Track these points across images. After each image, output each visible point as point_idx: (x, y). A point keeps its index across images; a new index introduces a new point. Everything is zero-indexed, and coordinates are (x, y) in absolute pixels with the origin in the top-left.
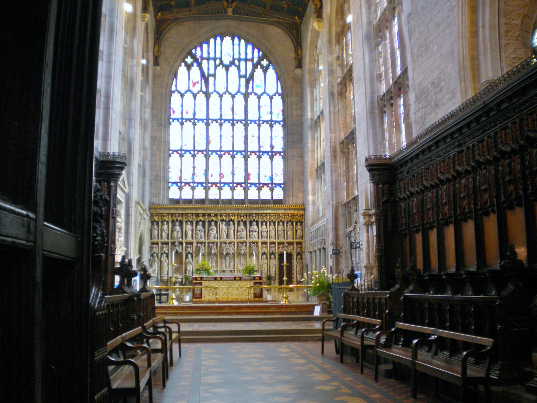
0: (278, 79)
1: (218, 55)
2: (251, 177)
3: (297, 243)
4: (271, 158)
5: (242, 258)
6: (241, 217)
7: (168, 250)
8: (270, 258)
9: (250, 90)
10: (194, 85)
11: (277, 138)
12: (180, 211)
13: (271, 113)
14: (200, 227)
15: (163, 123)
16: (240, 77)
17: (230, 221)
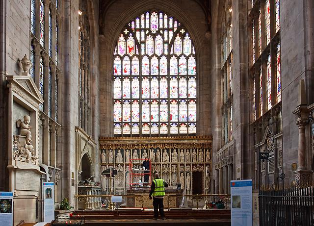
0: (192, 43)
1: (148, 27)
2: (172, 117)
4: (187, 103)
8: (187, 175)
9: (172, 53)
10: (130, 51)
11: (191, 88)
13: (187, 70)
16: (164, 42)
17: (157, 149)
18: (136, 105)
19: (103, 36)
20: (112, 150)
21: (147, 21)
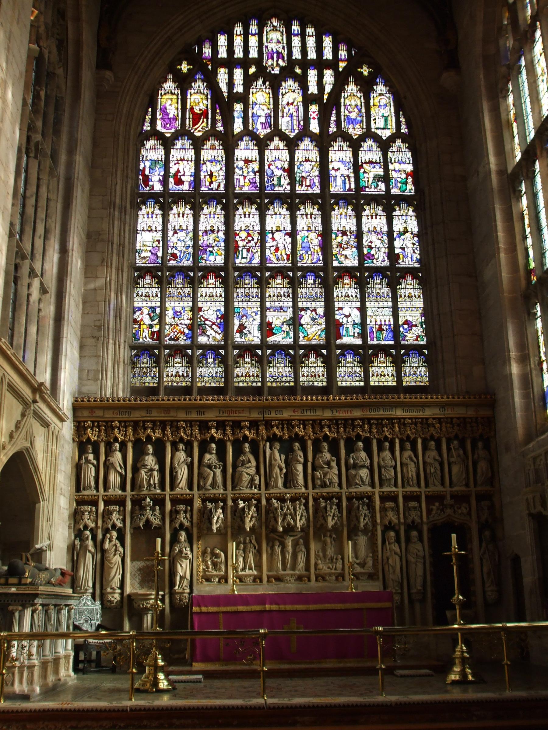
1: (253, 54)
2: (343, 331)
3: (480, 497)
4: (393, 285)
5: (328, 540)
6: (322, 427)
7: (124, 521)
8: (408, 540)
9: (333, 129)
10: (195, 121)
12: (156, 415)
14: (210, 458)
15: (118, 201)
16: (308, 100)
18: (211, 289)
19: (108, 74)
20: (123, 445)
21: (253, 41)
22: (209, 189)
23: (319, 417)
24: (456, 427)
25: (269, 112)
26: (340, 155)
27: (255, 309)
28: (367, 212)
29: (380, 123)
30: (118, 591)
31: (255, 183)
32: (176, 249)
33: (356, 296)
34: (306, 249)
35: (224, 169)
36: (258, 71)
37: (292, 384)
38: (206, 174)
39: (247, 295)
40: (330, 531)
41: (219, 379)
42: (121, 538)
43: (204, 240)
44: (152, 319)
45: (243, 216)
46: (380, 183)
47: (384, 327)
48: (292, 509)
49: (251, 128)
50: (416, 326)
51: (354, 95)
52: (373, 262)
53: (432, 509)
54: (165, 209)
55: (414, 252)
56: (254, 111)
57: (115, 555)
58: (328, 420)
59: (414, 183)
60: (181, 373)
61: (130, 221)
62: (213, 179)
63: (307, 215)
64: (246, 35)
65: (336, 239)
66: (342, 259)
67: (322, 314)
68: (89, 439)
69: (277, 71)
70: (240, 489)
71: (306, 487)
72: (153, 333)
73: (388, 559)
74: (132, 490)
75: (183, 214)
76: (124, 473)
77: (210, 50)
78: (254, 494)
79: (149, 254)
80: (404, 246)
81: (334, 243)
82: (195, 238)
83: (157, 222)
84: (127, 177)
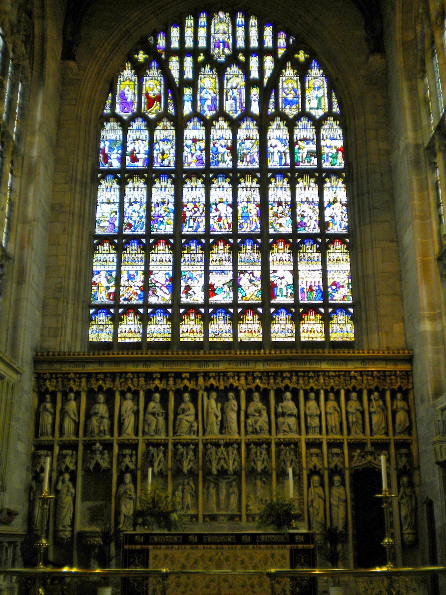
1: (202, 44)
2: (277, 292)
3: (399, 445)
4: (323, 249)
6: (254, 379)
8: (331, 484)
9: (271, 110)
14: (154, 406)
16: (250, 84)
19: (72, 64)
21: (202, 32)
22: (161, 166)
23: (252, 370)
24: (376, 380)
25: (215, 95)
26: (278, 133)
27: (199, 273)
28: (301, 184)
29: (314, 104)
30: (70, 529)
31: (202, 159)
32: (131, 219)
33: (289, 260)
34: (246, 218)
35: (174, 147)
36: (205, 58)
37: (231, 339)
38: (158, 152)
39: (193, 260)
40: (259, 474)
41: (166, 335)
42: (73, 479)
43: (155, 211)
44: (109, 282)
45: (190, 189)
46: (313, 158)
47: (314, 288)
48: (225, 453)
49: (198, 109)
50: (343, 286)
51: (291, 79)
52: (305, 229)
53: (354, 456)
54: (122, 183)
55: (342, 220)
56: (202, 95)
57: (67, 495)
58: (259, 372)
59: (344, 158)
60: (133, 330)
61: (91, 193)
62: (165, 157)
63: (246, 188)
64: (196, 26)
65: (272, 209)
66: (277, 227)
67: (259, 277)
68: (47, 389)
69: (222, 59)
70: (180, 435)
71: (239, 433)
72: (109, 294)
73: (312, 501)
74: (85, 436)
75: (138, 188)
76: (77, 420)
77: (164, 41)
78: (192, 440)
79: (107, 224)
80: (333, 215)
81: (271, 213)
82: (148, 209)
83: (115, 195)
84: (88, 155)
